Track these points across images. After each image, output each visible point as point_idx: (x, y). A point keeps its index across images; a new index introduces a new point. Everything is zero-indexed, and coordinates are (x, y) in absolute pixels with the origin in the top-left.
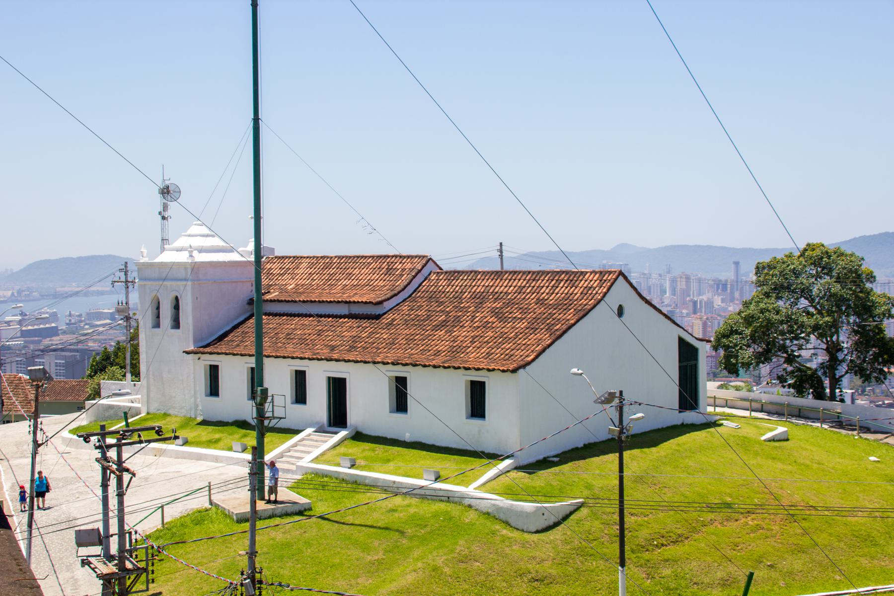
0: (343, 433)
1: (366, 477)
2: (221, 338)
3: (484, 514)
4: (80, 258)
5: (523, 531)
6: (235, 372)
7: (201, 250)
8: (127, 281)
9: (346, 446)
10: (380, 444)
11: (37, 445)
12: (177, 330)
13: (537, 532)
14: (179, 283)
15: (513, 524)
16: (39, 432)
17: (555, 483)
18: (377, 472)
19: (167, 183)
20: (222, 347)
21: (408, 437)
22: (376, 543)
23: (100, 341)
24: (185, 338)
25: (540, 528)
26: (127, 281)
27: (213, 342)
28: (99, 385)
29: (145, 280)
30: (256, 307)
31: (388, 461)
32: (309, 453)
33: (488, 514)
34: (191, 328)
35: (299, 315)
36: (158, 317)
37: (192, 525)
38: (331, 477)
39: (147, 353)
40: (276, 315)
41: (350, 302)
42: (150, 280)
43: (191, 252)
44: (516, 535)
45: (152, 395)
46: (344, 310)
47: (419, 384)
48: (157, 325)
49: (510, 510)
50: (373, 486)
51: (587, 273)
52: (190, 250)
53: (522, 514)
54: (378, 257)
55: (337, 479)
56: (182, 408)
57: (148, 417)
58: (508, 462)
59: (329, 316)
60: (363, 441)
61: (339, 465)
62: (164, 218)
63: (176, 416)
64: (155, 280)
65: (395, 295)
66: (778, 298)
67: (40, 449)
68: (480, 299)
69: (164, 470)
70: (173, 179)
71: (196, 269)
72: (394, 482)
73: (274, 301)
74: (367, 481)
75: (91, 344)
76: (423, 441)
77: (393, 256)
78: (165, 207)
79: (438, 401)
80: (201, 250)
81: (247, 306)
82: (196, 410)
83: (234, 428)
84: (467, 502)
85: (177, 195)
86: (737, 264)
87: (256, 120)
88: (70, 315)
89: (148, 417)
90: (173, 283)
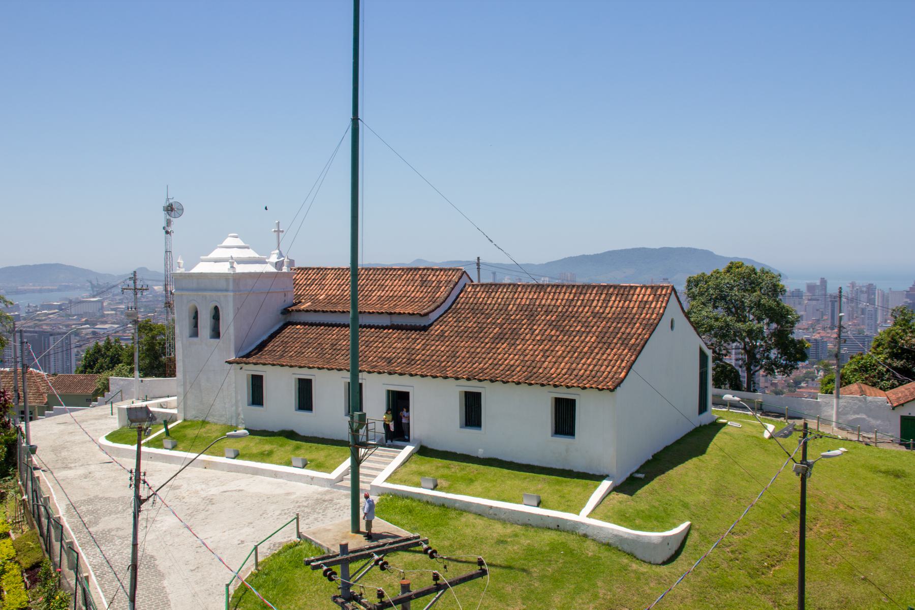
0: (409, 449)
1: (456, 501)
2: (261, 347)
3: (604, 544)
4: (35, 266)
5: (650, 563)
6: (280, 384)
7: (242, 261)
8: (135, 289)
9: (415, 462)
10: (452, 460)
11: (139, 501)
12: (218, 340)
13: (664, 563)
14: (219, 294)
15: (639, 556)
16: (141, 485)
17: (656, 504)
18: (465, 494)
19: (171, 201)
20: (265, 357)
21: (481, 453)
22: (509, 589)
23: (51, 325)
24: (227, 346)
25: (665, 559)
26: (135, 289)
27: (255, 351)
28: (108, 380)
29: (183, 289)
30: (289, 316)
31: (471, 481)
32: (381, 470)
33: (609, 545)
34: (232, 338)
35: (337, 325)
36: (196, 326)
37: (290, 568)
38: (412, 499)
39: (183, 361)
40: (312, 325)
41: (391, 314)
42: (188, 290)
43: (232, 263)
44: (644, 568)
45: (189, 402)
46: (386, 321)
47: (494, 400)
48: (195, 334)
49: (636, 541)
50: (465, 509)
51: (637, 287)
52: (232, 261)
53: (648, 545)
54: (407, 269)
55: (419, 501)
56: (222, 416)
57: (186, 423)
58: (606, 485)
59: (371, 327)
60: (431, 457)
61: (418, 485)
62: (167, 232)
63: (216, 424)
64: (192, 290)
65: (438, 307)
66: (715, 307)
67: (144, 507)
68: (530, 312)
69: (225, 488)
70: (176, 198)
71: (239, 279)
72: (491, 507)
73: (307, 311)
74: (457, 505)
75: (44, 327)
76: (500, 458)
77: (424, 269)
78: (169, 223)
79: (518, 419)
80: (242, 261)
81: (281, 316)
82: (237, 418)
83: (282, 439)
84: (581, 531)
85: (180, 212)
86: (494, 273)
87: (355, 120)
88: (29, 306)
89: (186, 423)
90: (214, 294)
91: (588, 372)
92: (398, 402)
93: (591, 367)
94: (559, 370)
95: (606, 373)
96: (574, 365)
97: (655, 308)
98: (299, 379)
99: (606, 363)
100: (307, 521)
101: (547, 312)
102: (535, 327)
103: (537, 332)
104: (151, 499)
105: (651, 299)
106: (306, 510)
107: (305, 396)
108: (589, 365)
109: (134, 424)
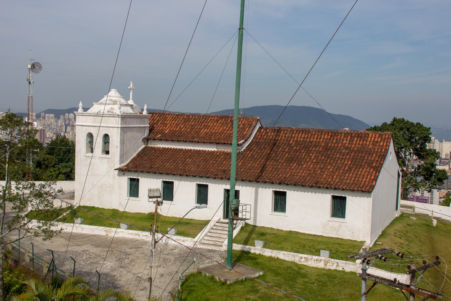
95: (363, 182)
97: (383, 145)
103: (313, 157)
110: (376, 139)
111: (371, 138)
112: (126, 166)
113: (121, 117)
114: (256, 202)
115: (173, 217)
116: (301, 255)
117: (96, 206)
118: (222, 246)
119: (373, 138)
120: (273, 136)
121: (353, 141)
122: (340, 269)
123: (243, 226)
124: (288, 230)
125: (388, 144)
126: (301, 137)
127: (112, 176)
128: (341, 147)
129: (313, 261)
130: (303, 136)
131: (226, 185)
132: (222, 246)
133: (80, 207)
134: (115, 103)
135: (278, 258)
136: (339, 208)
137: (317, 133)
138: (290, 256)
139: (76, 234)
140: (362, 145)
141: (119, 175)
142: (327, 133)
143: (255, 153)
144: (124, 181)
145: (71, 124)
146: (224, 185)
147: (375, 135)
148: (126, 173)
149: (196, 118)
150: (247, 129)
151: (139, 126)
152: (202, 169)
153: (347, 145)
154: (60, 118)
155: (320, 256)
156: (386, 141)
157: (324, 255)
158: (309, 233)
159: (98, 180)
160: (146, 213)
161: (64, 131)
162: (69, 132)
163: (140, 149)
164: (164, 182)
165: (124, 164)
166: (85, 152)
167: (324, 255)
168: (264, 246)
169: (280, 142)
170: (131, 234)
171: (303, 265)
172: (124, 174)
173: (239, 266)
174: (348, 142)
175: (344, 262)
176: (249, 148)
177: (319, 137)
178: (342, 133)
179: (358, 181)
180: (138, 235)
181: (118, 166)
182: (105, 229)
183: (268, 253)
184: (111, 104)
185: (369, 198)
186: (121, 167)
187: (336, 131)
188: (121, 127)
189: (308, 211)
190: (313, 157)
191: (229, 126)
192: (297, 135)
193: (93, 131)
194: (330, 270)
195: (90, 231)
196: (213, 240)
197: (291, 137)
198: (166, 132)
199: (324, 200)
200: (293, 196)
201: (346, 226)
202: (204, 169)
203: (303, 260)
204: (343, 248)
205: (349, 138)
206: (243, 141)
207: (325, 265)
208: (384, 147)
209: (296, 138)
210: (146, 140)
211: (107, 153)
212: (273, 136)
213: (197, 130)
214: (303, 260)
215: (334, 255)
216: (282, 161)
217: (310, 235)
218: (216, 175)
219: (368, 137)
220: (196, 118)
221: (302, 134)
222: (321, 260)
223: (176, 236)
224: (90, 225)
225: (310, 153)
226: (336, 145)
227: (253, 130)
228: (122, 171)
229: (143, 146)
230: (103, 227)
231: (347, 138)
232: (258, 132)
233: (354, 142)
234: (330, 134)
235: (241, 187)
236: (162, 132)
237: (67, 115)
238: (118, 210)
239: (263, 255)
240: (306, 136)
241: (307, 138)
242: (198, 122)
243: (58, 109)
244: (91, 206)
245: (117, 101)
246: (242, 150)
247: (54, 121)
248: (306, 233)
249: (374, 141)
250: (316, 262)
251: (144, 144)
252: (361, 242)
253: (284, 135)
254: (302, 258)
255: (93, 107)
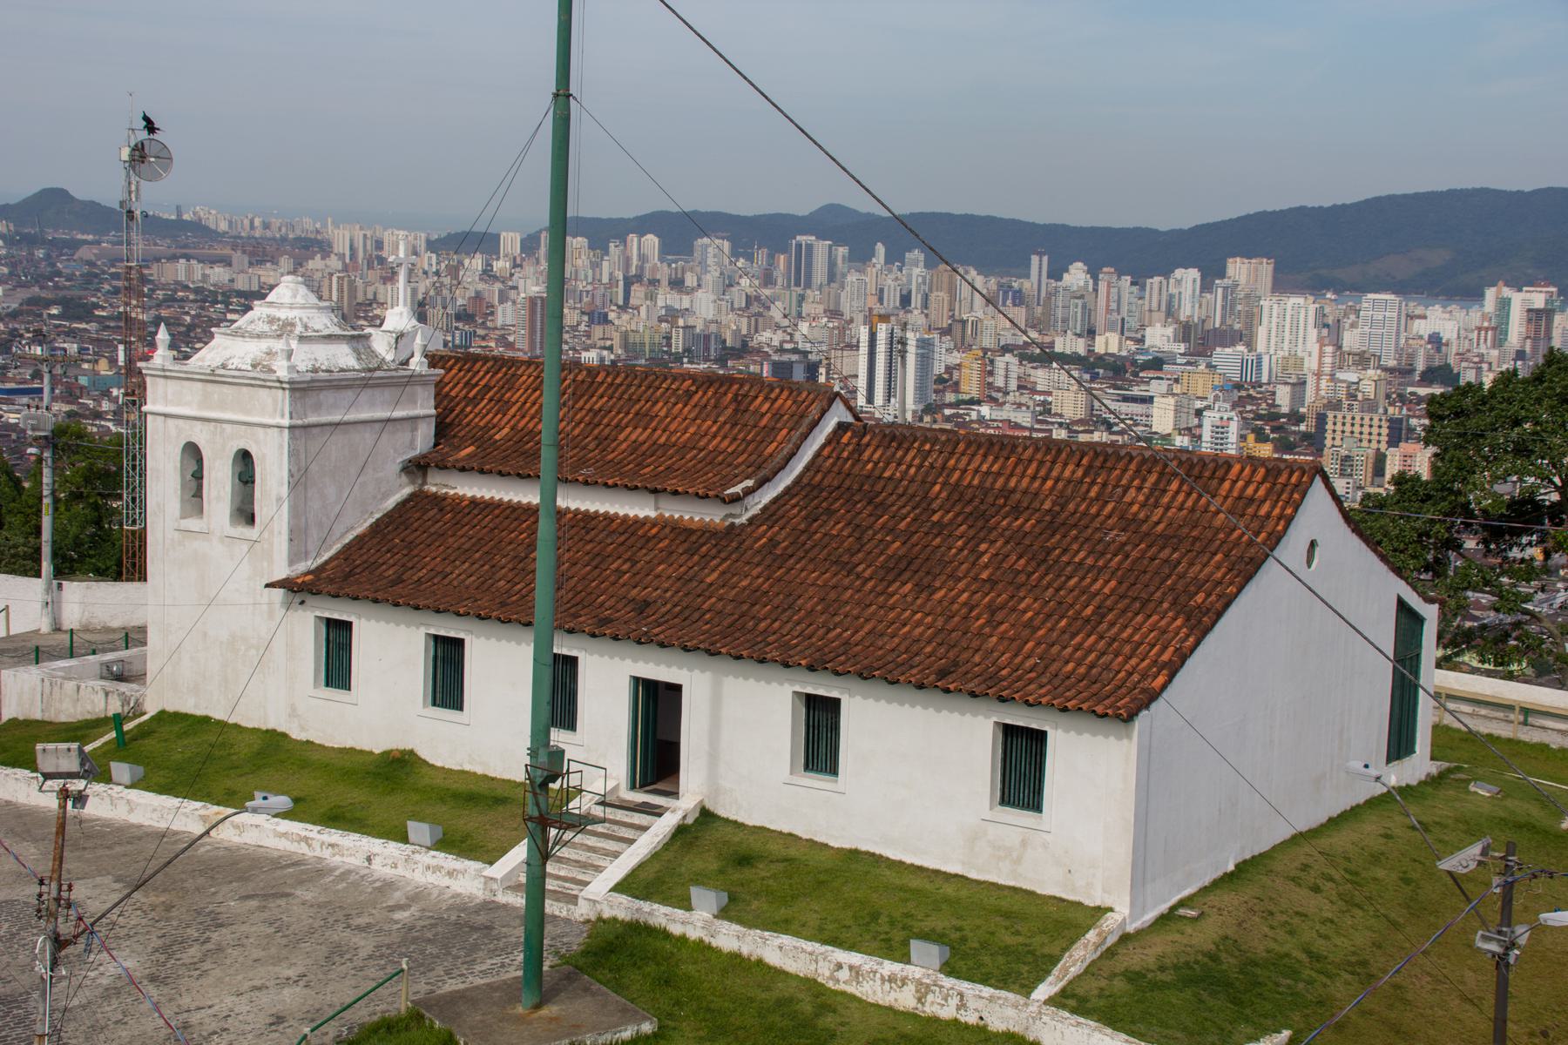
91: (1082, 670)
92: (657, 710)
93: (1092, 657)
94: (1018, 660)
95: (1122, 674)
96: (1055, 649)
97: (1268, 516)
98: (436, 638)
99: (1127, 649)
100: (1205, 995)
101: (1017, 511)
102: (983, 547)
103: (985, 559)
104: (82, 940)
105: (1261, 492)
106: (430, 949)
107: (447, 679)
108: (1090, 651)
109: (49, 783)
110: (1250, 491)
111: (1235, 482)
112: (309, 573)
113: (292, 390)
114: (740, 730)
115: (463, 772)
116: (841, 955)
117: (218, 714)
118: (573, 900)
119: (1240, 484)
120: (876, 464)
121: (1164, 491)
122: (970, 1018)
123: (690, 821)
124: (847, 846)
125: (1289, 511)
126: (977, 471)
127: (265, 607)
128: (1109, 517)
129: (879, 982)
130: (984, 468)
131: (635, 661)
132: (573, 900)
133: (163, 717)
134: (285, 328)
135: (760, 962)
136: (1022, 773)
137: (1039, 456)
138: (802, 956)
139: (107, 823)
140: (1192, 510)
141: (288, 606)
142: (1075, 459)
143: (783, 533)
144: (302, 630)
145: (647, 275)
146: (628, 662)
147: (1254, 472)
148: (310, 600)
149: (618, 381)
150: (784, 432)
151: (385, 414)
152: (570, 595)
153: (1135, 508)
154: (607, 253)
155: (908, 962)
156: (1284, 497)
157: (925, 960)
158: (918, 862)
159: (215, 615)
160: (377, 751)
161: (621, 302)
162: (637, 308)
163: (390, 503)
164: (437, 639)
165: (302, 567)
166: (178, 513)
167: (925, 960)
168: (724, 914)
169: (896, 487)
170: (285, 835)
171: (843, 993)
172: (302, 603)
173: (586, 990)
174: (1141, 498)
175: (987, 991)
176: (771, 513)
177: (1042, 473)
178: (1132, 459)
179: (1107, 667)
180: (306, 840)
181: (282, 572)
182: (202, 812)
183: (730, 938)
184: (267, 336)
185: (1125, 741)
186: (293, 575)
187: (1110, 451)
188: (291, 428)
189: (911, 779)
190: (985, 559)
191: (722, 419)
192: (965, 460)
193: (200, 435)
194: (934, 1020)
195: (154, 816)
196: (562, 873)
197: (943, 467)
198: (497, 437)
199: (967, 737)
200: (867, 717)
201: (1045, 846)
202: (614, 590)
203: (844, 974)
204: (1018, 933)
205: (1152, 478)
206: (750, 483)
207: (919, 1000)
208: (1270, 524)
209: (957, 474)
210: (417, 467)
211: (250, 519)
212: (876, 464)
213: (607, 431)
214: (844, 974)
215: (963, 962)
216: (867, 574)
217: (920, 869)
218: (606, 621)
219: (1223, 480)
220: (618, 381)
221: (985, 456)
222: (904, 981)
223: (433, 853)
224: (161, 793)
225: (983, 540)
226: (1093, 511)
227: (805, 436)
228: (297, 589)
229: (408, 490)
230: (198, 804)
231: (1144, 480)
232: (828, 442)
233: (1166, 500)
234: (1085, 461)
235: (685, 672)
236: (482, 439)
237: (633, 239)
238: (284, 735)
239: (709, 947)
240: (995, 468)
241: (999, 474)
242: (620, 399)
243: (605, 216)
244: (199, 713)
245: (293, 325)
246: (744, 519)
247: (587, 262)
248: (908, 860)
249: (1240, 498)
250: (887, 986)
251: (413, 482)
252: (1099, 908)
253: (917, 461)
254: (839, 966)
255: (212, 344)
